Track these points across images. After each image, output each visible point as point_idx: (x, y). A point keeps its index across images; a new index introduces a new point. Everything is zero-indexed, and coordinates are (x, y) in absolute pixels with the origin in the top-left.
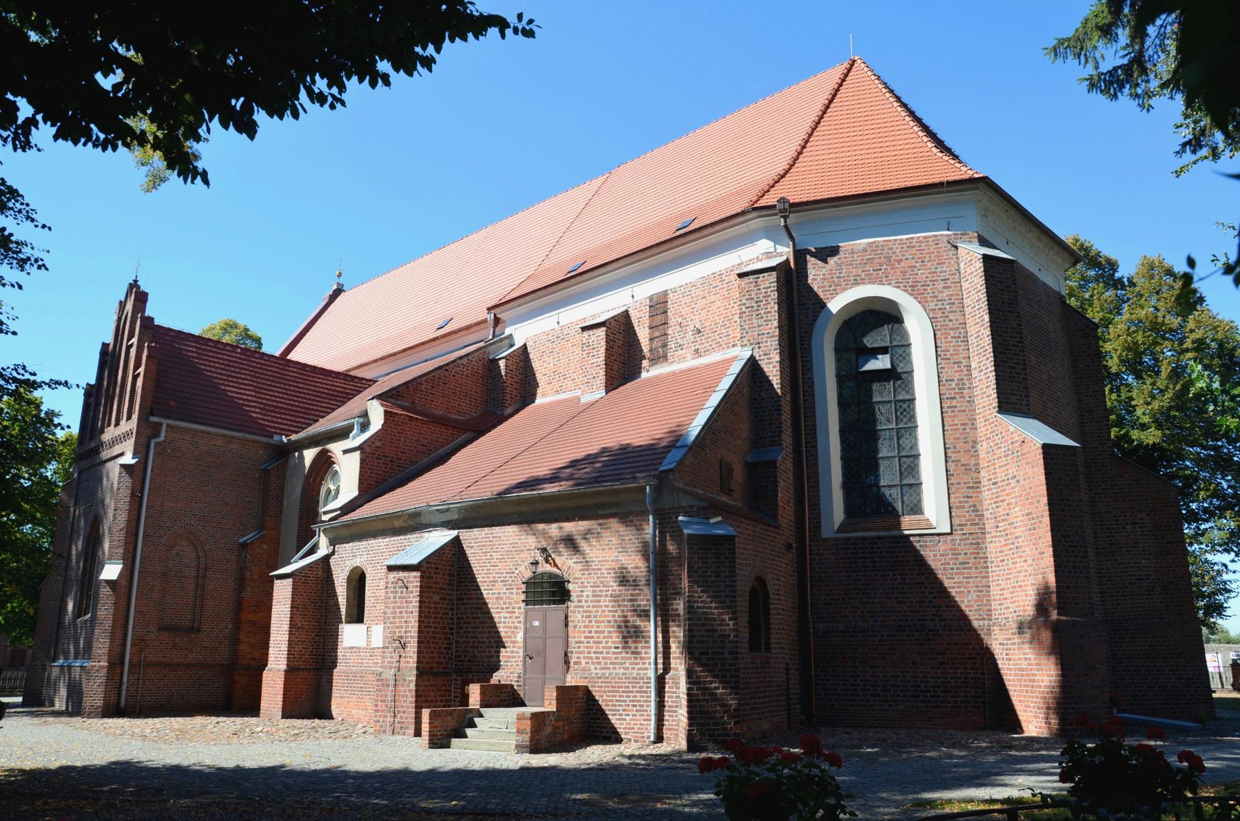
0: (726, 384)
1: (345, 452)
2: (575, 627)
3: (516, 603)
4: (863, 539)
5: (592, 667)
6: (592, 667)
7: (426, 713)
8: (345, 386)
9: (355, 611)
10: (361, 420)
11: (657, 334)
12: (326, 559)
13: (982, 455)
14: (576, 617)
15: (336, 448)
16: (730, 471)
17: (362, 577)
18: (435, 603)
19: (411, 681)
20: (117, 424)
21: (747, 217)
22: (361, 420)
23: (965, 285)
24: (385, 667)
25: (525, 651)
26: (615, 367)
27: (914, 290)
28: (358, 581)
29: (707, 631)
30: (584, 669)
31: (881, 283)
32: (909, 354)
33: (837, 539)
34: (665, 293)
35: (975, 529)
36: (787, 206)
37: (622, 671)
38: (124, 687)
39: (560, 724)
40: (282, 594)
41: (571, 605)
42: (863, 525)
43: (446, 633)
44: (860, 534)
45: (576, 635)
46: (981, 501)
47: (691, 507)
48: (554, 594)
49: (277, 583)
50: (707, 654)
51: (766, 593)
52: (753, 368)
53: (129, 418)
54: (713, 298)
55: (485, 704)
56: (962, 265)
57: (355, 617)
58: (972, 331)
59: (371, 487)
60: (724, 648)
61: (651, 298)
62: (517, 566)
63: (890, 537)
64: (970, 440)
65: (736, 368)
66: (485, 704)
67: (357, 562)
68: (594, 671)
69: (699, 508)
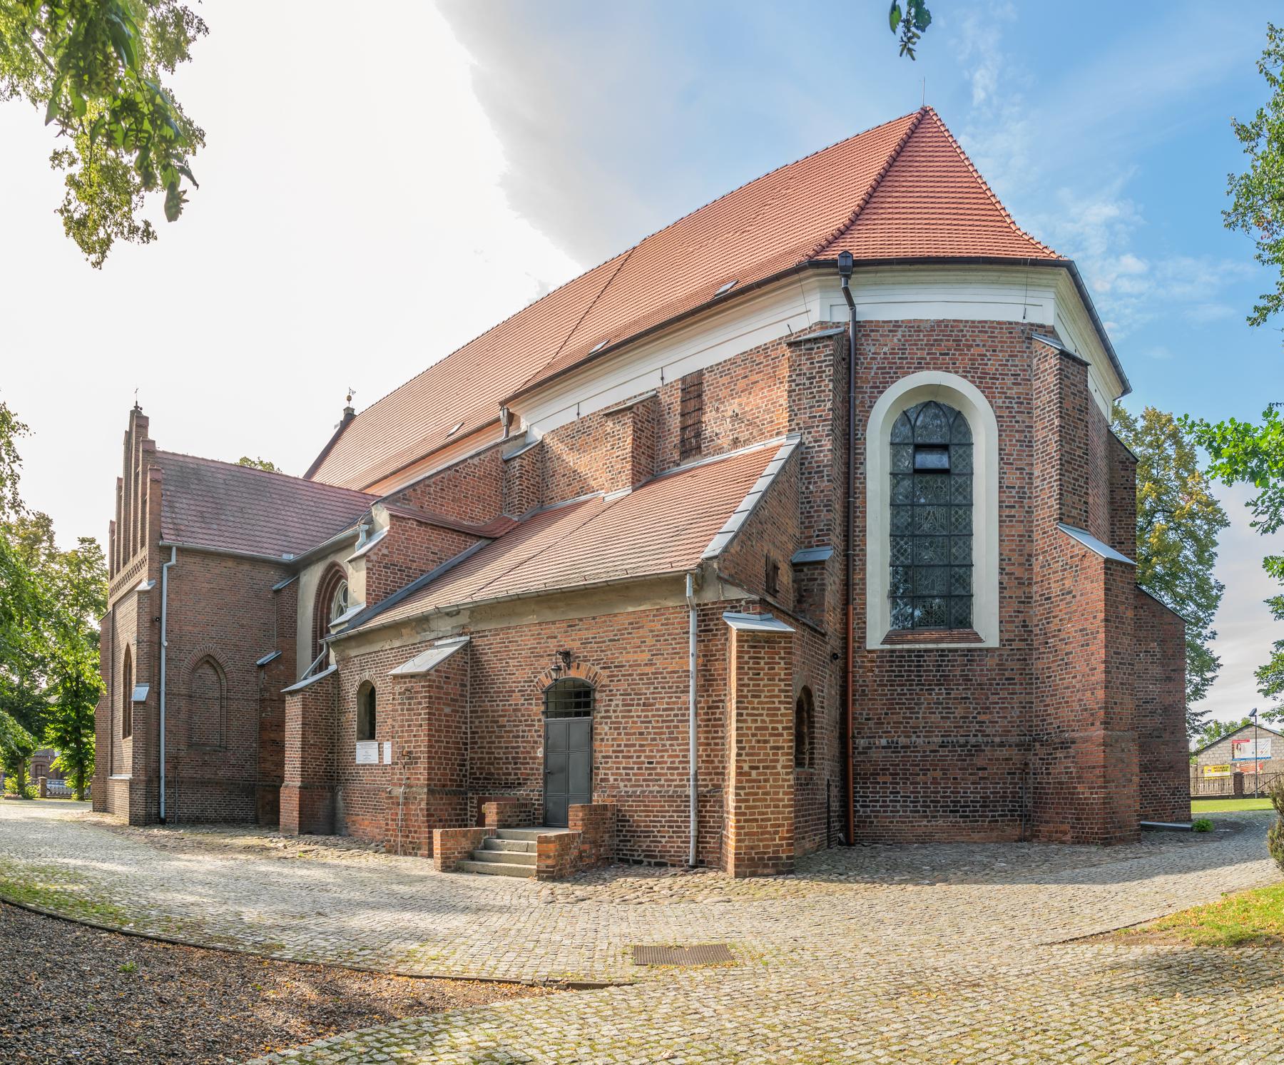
0: (773, 468)
1: (350, 562)
2: (602, 740)
3: (536, 714)
4: (909, 651)
5: (622, 784)
6: (622, 784)
7: (437, 833)
8: (356, 505)
9: (367, 727)
10: (367, 527)
11: (690, 422)
12: (336, 674)
13: (1036, 569)
14: (603, 729)
15: (343, 559)
16: (776, 568)
17: (373, 691)
18: (446, 715)
19: (422, 800)
20: (135, 552)
21: (802, 275)
22: (367, 527)
23: (1037, 384)
24: (394, 785)
25: (546, 767)
26: (643, 462)
27: (984, 382)
28: (368, 695)
29: (758, 742)
30: (613, 787)
31: (947, 370)
32: (970, 456)
33: (882, 651)
34: (700, 373)
35: (1022, 645)
36: (850, 263)
37: (657, 788)
38: (162, 799)
39: (587, 846)
40: (294, 710)
41: (598, 716)
42: (910, 637)
43: (460, 749)
44: (906, 646)
45: (603, 748)
46: (1030, 617)
47: (738, 601)
48: (578, 705)
49: (288, 698)
50: (758, 768)
51: (811, 704)
52: (800, 457)
53: (143, 545)
54: (756, 377)
55: (504, 824)
56: (1035, 361)
57: (367, 734)
58: (1039, 435)
59: (381, 599)
60: (778, 761)
61: (683, 379)
62: (536, 673)
63: (937, 650)
64: (1025, 552)
65: (784, 453)
66: (504, 824)
67: (366, 676)
68: (623, 789)
69: (748, 603)
